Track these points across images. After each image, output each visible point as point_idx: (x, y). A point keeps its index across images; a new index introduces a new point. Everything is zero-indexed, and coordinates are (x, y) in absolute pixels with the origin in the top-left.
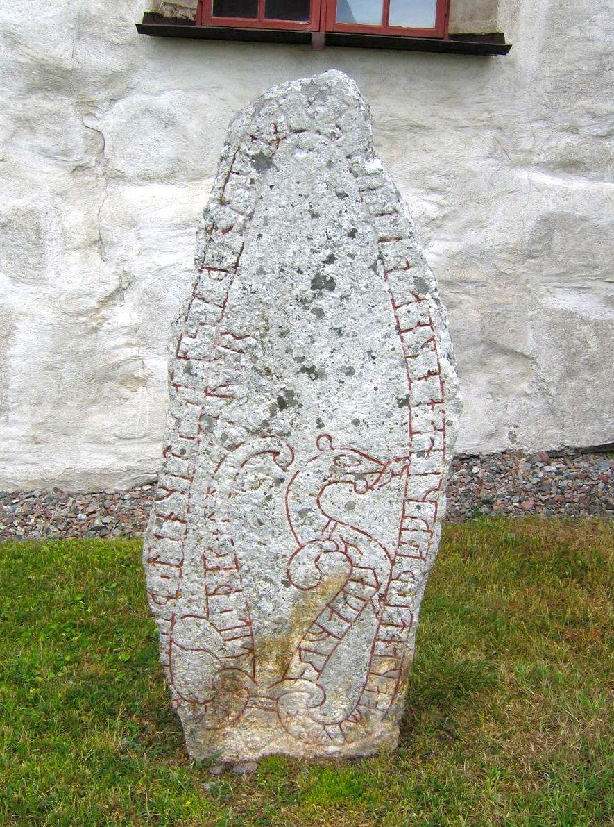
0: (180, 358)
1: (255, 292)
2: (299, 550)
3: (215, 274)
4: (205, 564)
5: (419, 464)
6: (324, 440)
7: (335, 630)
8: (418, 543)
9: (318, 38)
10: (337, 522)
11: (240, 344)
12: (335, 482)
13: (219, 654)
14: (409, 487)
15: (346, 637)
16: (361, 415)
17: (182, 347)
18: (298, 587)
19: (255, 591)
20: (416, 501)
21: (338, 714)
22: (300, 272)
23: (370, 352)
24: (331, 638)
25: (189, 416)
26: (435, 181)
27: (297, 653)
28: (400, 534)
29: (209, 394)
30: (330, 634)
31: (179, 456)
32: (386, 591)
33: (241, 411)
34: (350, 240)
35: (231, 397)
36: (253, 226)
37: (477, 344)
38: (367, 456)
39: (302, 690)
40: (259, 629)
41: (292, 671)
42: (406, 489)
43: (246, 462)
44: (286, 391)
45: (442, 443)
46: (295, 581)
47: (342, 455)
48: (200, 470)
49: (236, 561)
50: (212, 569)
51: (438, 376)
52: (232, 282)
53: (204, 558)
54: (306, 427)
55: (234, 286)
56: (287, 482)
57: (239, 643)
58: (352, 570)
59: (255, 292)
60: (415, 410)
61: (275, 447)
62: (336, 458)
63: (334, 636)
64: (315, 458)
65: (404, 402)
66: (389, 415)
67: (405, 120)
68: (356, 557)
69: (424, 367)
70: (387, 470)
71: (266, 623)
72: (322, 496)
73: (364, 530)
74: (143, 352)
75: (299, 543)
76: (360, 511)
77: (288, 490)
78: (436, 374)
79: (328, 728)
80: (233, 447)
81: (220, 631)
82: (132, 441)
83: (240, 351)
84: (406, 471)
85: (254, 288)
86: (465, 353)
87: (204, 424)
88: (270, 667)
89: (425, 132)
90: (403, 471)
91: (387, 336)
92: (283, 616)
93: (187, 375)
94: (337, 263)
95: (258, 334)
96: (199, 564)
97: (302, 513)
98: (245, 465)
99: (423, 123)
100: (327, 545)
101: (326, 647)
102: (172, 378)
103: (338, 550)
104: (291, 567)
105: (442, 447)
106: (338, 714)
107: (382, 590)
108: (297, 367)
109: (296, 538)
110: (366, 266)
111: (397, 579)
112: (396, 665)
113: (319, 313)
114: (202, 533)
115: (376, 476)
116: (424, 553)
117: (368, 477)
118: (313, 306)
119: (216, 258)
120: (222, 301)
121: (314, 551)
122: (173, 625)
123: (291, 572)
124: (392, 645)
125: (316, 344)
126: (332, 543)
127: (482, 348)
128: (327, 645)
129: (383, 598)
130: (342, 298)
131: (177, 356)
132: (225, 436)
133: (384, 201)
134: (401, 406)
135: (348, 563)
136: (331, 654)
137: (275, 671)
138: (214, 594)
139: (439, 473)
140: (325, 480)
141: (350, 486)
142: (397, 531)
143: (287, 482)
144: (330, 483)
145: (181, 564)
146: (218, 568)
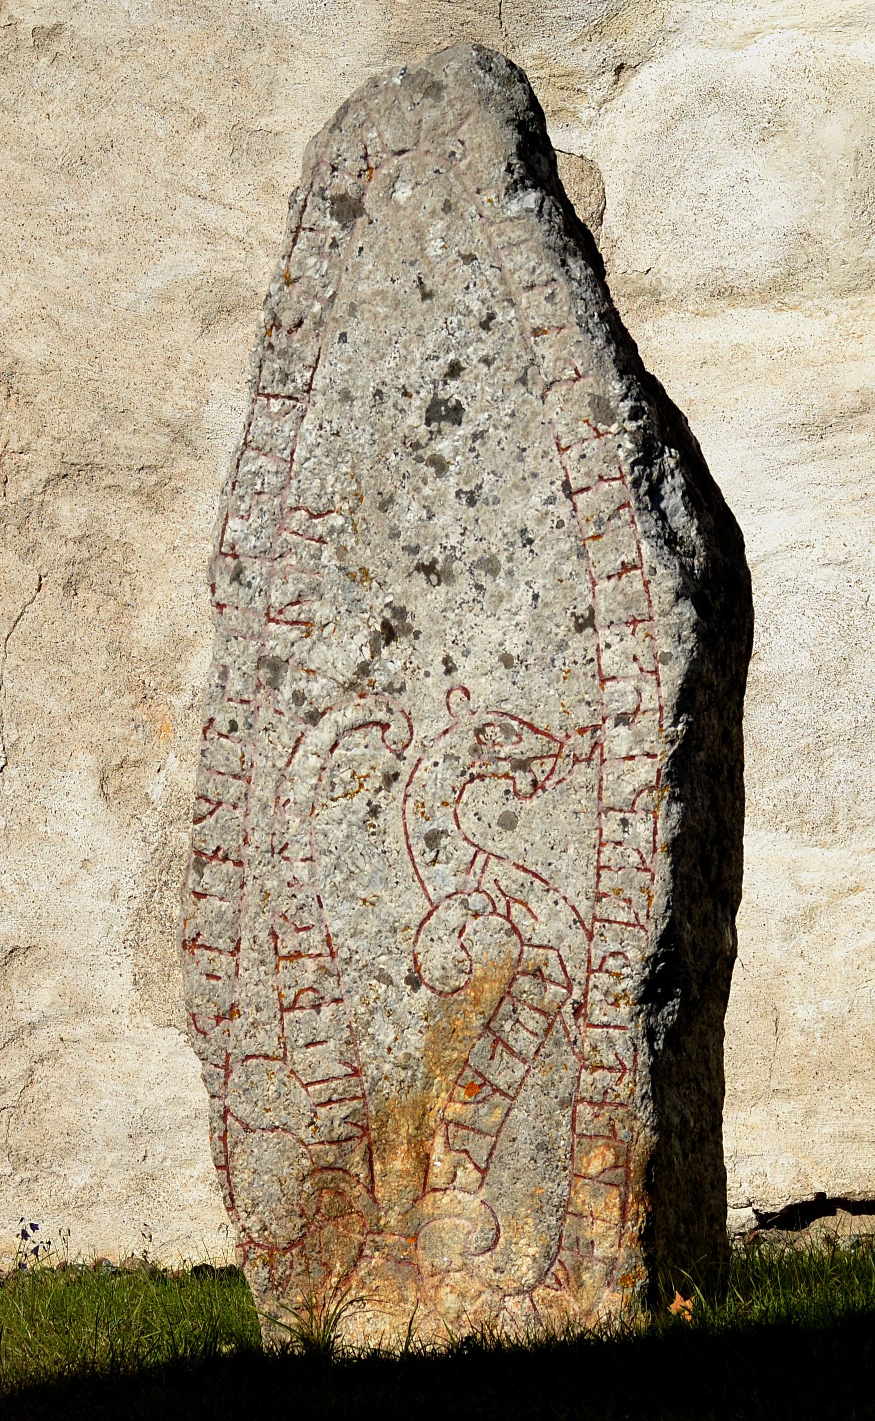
0: (226, 555)
1: (337, 434)
2: (430, 914)
3: (275, 406)
4: (276, 948)
5: (619, 740)
6: (457, 695)
7: (501, 1081)
8: (628, 893)
11: (320, 527)
12: (482, 777)
13: (305, 1134)
14: (604, 783)
15: (523, 1094)
16: (514, 646)
17: (228, 537)
18: (433, 989)
19: (364, 1002)
20: (621, 811)
21: (524, 1269)
22: (406, 394)
23: (524, 531)
25: (241, 660)
27: (441, 1132)
29: (273, 620)
31: (227, 737)
32: (585, 995)
33: (325, 648)
34: (484, 335)
35: (306, 625)
36: (334, 319)
38: (531, 726)
39: (458, 1213)
40: (375, 1082)
41: (436, 1170)
42: (600, 787)
43: (335, 745)
44: (394, 609)
45: (656, 697)
46: (426, 977)
47: (489, 725)
48: (260, 762)
49: (328, 941)
50: (289, 957)
51: (638, 572)
52: (303, 417)
53: (274, 935)
54: (427, 674)
55: (306, 425)
56: (404, 778)
57: (340, 1111)
58: (522, 952)
59: (337, 434)
60: (605, 636)
61: (381, 715)
62: (479, 731)
64: (446, 732)
65: (585, 622)
66: (562, 646)
68: (525, 924)
70: (565, 751)
71: (387, 1067)
72: (461, 805)
73: (533, 869)
75: (429, 900)
76: (524, 832)
77: (407, 796)
78: (635, 567)
80: (314, 718)
81: (306, 1086)
83: (321, 540)
84: (597, 752)
85: (335, 426)
87: (264, 674)
88: (398, 1165)
90: (592, 752)
91: (551, 500)
92: (411, 1050)
93: (235, 584)
94: (466, 376)
96: (266, 947)
97: (432, 839)
98: (336, 751)
100: (476, 901)
101: (490, 1118)
103: (494, 912)
104: (419, 948)
105: (654, 704)
106: (524, 1269)
107: (577, 993)
108: (406, 561)
109: (425, 889)
110: (511, 377)
111: (600, 969)
112: (617, 1157)
113: (440, 465)
114: (269, 885)
115: (549, 763)
116: (642, 914)
117: (535, 766)
118: (427, 454)
119: (277, 376)
120: (288, 452)
121: (453, 915)
122: (227, 1076)
123: (420, 957)
124: (606, 1112)
125: (435, 520)
126: (484, 896)
128: (490, 1113)
129: (579, 1010)
130: (475, 437)
131: (221, 553)
132: (298, 698)
133: (532, 264)
134: (580, 628)
135: (515, 937)
136: (499, 1131)
137: (407, 1172)
138: (292, 1008)
139: (655, 756)
140: (463, 773)
141: (505, 784)
142: (592, 871)
143: (404, 778)
144: (472, 780)
145: (237, 948)
146: (298, 955)
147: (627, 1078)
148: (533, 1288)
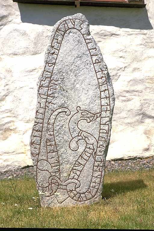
5: (104, 114)
6: (78, 108)
7: (82, 163)
9: (77, 3)
10: (82, 131)
11: (56, 83)
24: (82, 166)
26: (121, 54)
28: (99, 134)
30: (81, 164)
37: (140, 115)
63: (82, 165)
67: (109, 32)
68: (88, 141)
69: (104, 88)
74: (14, 119)
79: (81, 195)
82: (9, 154)
86: (135, 118)
89: (117, 36)
95: (61, 80)
99: (116, 33)
102: (39, 92)
107: (95, 151)
124: (99, 168)
127: (141, 116)
138: (49, 153)
147: (102, 163)
148: (85, 193)
